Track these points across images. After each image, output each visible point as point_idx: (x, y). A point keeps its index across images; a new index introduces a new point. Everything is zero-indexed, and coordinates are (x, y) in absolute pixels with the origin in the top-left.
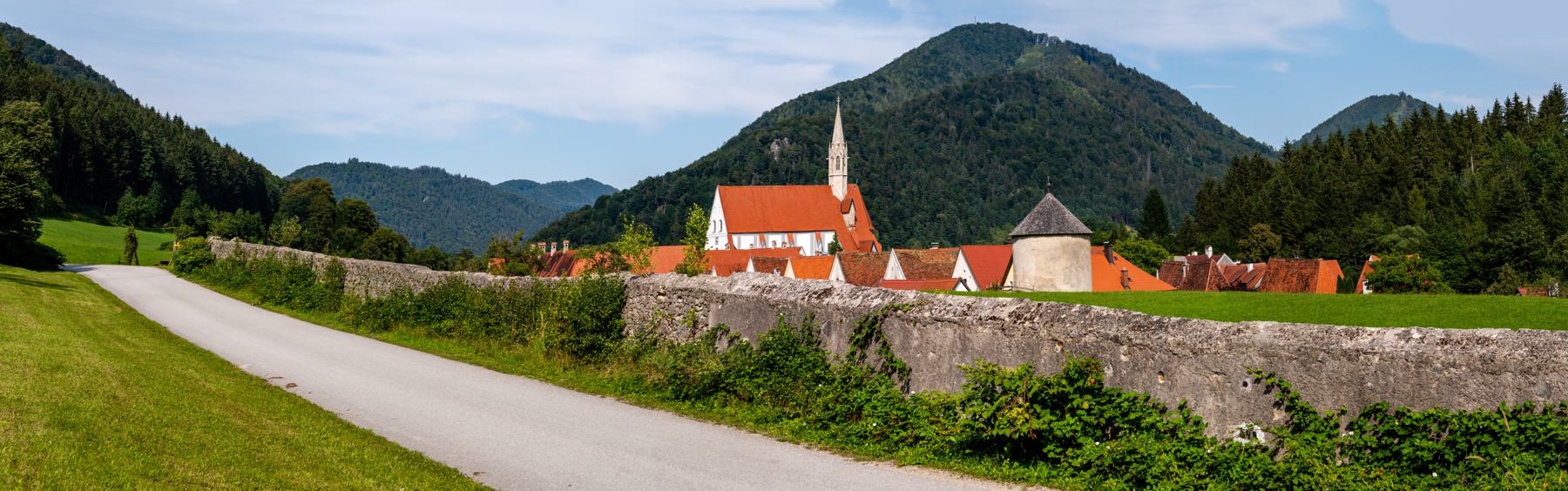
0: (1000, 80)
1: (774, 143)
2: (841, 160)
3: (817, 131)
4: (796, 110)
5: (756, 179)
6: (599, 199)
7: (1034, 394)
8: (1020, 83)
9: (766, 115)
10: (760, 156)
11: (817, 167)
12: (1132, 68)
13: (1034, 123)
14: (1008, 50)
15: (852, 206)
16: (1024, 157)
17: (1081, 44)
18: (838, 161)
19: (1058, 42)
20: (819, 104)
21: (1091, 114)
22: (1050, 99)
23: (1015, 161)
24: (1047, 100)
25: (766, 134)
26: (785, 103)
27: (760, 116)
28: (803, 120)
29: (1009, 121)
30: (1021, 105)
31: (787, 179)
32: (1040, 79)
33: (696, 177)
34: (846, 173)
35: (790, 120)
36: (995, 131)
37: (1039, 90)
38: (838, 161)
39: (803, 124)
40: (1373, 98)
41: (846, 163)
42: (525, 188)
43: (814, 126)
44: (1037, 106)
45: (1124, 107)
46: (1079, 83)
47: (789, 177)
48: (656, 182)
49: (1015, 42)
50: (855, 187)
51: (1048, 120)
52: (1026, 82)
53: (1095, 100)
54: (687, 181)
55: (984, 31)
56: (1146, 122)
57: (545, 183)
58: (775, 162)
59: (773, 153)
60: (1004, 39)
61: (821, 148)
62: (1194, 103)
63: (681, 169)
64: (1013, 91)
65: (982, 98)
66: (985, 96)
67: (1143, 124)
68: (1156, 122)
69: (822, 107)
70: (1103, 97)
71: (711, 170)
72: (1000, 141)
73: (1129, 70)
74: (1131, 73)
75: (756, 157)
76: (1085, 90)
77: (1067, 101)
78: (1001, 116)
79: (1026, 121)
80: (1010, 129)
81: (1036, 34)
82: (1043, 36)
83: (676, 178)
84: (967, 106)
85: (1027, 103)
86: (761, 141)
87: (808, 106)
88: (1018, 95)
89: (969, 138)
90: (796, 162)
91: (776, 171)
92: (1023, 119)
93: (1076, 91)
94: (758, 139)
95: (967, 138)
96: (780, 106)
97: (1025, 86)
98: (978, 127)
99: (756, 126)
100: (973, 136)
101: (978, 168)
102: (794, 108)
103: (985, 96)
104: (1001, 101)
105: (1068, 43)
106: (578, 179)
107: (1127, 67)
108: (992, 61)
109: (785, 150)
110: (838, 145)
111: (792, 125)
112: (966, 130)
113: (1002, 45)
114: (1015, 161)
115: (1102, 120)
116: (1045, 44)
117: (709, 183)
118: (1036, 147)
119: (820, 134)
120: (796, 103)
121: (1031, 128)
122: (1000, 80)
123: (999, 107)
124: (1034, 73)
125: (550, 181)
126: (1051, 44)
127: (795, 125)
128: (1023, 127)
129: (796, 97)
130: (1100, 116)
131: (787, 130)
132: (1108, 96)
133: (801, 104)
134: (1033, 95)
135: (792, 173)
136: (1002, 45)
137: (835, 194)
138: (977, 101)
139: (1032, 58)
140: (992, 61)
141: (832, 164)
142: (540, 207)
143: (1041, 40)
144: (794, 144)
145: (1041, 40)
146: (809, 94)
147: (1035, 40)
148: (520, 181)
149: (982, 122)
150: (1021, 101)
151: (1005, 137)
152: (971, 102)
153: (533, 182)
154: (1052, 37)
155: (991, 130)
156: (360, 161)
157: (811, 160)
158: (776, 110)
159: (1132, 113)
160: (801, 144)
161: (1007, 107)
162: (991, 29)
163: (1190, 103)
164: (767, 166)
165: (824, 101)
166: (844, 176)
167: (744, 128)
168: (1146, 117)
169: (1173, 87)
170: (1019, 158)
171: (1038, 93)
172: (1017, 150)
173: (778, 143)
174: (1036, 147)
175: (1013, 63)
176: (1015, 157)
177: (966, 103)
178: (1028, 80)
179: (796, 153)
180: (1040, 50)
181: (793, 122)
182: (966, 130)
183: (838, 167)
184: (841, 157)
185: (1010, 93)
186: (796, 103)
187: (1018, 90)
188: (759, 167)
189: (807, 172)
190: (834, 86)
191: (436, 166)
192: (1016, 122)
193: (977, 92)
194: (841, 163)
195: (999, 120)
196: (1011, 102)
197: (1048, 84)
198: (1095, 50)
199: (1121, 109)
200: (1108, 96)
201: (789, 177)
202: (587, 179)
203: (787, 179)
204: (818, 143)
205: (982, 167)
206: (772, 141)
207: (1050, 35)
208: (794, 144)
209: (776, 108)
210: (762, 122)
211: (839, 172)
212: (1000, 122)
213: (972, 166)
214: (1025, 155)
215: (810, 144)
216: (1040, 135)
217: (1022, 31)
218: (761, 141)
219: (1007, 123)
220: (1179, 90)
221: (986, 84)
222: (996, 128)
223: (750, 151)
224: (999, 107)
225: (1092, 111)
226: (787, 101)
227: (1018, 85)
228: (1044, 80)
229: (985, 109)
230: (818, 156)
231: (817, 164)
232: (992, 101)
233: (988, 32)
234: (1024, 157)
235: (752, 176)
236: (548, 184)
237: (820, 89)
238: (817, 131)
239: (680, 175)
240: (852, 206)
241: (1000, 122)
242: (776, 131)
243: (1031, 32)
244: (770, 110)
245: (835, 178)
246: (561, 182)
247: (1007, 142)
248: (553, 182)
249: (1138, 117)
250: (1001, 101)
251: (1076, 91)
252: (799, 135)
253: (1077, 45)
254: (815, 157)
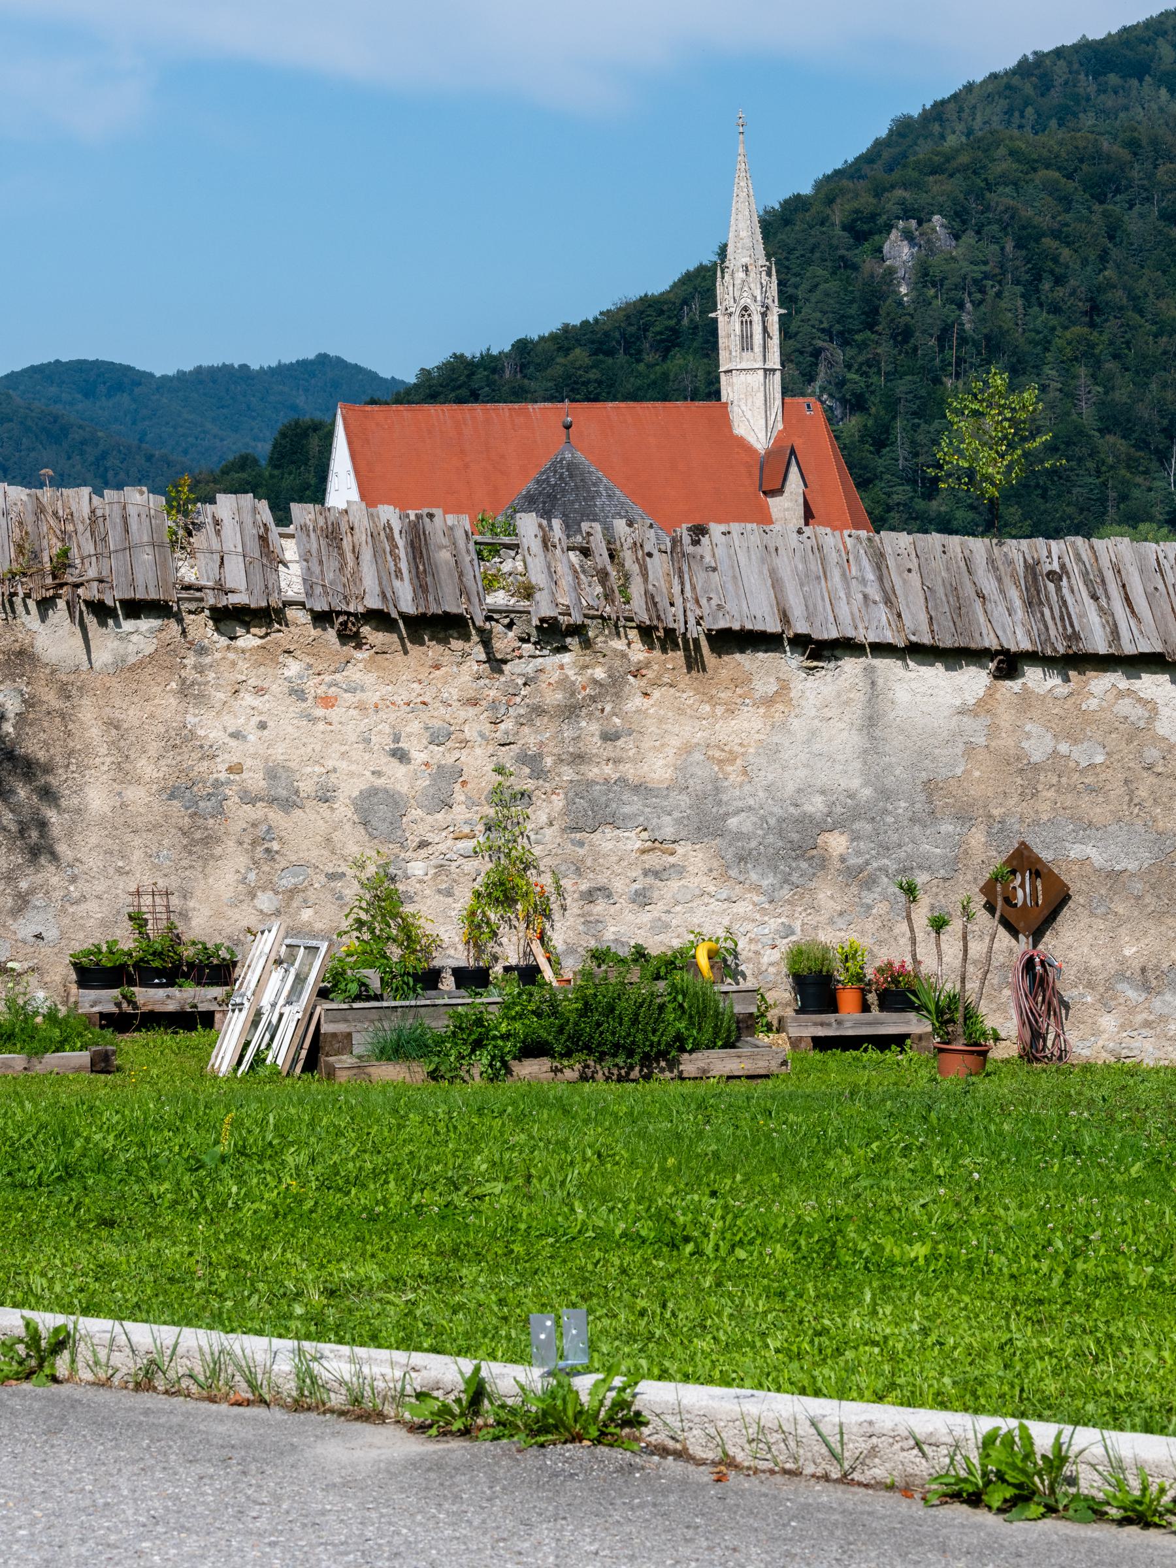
1: (894, 234)
2: (756, 318)
3: (1051, 189)
4: (1009, 112)
5: (830, 365)
6: (283, 435)
9: (904, 129)
10: (848, 281)
11: (1054, 320)
15: (794, 469)
18: (747, 324)
20: (1092, 89)
25: (866, 201)
26: (969, 87)
27: (883, 133)
28: (1002, 151)
31: (945, 364)
33: (621, 358)
34: (775, 361)
35: (957, 151)
38: (747, 324)
39: (1003, 165)
41: (774, 329)
42: (102, 389)
43: (1043, 174)
47: (952, 355)
48: (482, 373)
50: (812, 409)
54: (587, 369)
57: (171, 372)
58: (900, 303)
59: (891, 271)
61: (1066, 253)
63: (566, 329)
69: (1109, 101)
71: (674, 331)
75: (833, 286)
83: (550, 361)
86: (848, 227)
87: (1055, 97)
90: (977, 304)
91: (903, 336)
94: (837, 219)
96: (955, 97)
99: (866, 169)
102: (1003, 104)
106: (289, 358)
109: (933, 260)
110: (746, 269)
111: (965, 168)
117: (665, 376)
119: (1066, 202)
120: (1009, 87)
125: (188, 367)
127: (974, 169)
129: (1011, 63)
131: (941, 188)
133: (1028, 89)
135: (963, 340)
137: (740, 430)
141: (729, 330)
142: (149, 458)
144: (969, 238)
146: (1059, 53)
148: (80, 366)
153: (129, 368)
157: (1031, 293)
158: (938, 113)
160: (995, 240)
164: (870, 319)
165: (1113, 79)
166: (768, 372)
167: (828, 178)
173: (908, 236)
179: (976, 271)
181: (964, 159)
183: (746, 343)
184: (756, 310)
186: (1009, 87)
188: (842, 319)
189: (1018, 337)
190: (1149, 24)
194: (757, 329)
201: (952, 355)
202: (323, 359)
203: (945, 364)
204: (1056, 235)
206: (889, 227)
208: (969, 238)
209: (940, 105)
210: (886, 154)
211: (752, 360)
215: (1027, 238)
218: (848, 227)
223: (809, 262)
226: (979, 79)
230: (1059, 281)
231: (1055, 310)
235: (817, 353)
236: (181, 375)
237: (1096, 34)
238: (1051, 189)
239: (567, 351)
240: (794, 469)
242: (899, 193)
244: (915, 112)
245: (739, 380)
246: (226, 369)
248: (199, 370)
252: (988, 208)
254: (1046, 286)
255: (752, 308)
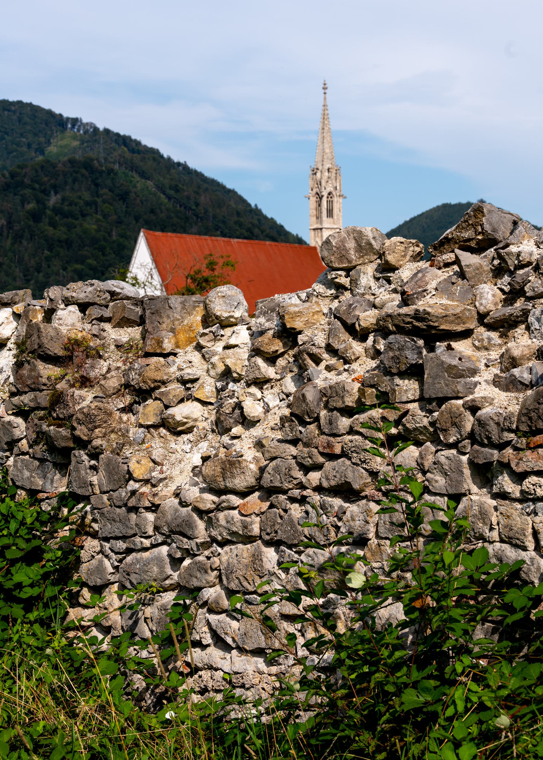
0: (54, 168)
7: (402, 634)
8: (77, 172)
12: (182, 161)
13: (98, 220)
14: (36, 135)
16: (90, 261)
17: (122, 133)
19: (96, 129)
21: (162, 212)
22: (113, 192)
23: (79, 266)
24: (110, 193)
29: (68, 218)
30: (80, 198)
32: (100, 168)
36: (51, 228)
37: (99, 181)
40: (446, 206)
44: (99, 200)
45: (197, 205)
46: (143, 175)
49: (44, 126)
51: (114, 217)
52: (84, 171)
53: (163, 196)
55: (4, 109)
56: (224, 222)
60: (28, 120)
62: (253, 205)
64: (70, 180)
65: (34, 189)
66: (37, 186)
67: (221, 225)
68: (236, 223)
70: (172, 193)
72: (60, 241)
73: (179, 164)
74: (181, 168)
76: (150, 183)
77: (132, 195)
78: (57, 211)
79: (88, 218)
80: (70, 227)
81: (68, 119)
82: (75, 121)
84: (17, 197)
85: (87, 196)
88: (77, 186)
89: (22, 237)
92: (84, 215)
93: (140, 183)
95: (18, 238)
97: (83, 175)
98: (31, 223)
100: (27, 234)
101: (36, 274)
103: (37, 186)
104: (56, 193)
105: (107, 131)
107: (176, 161)
108: (19, 149)
112: (17, 227)
113: (29, 127)
114: (79, 266)
115: (175, 220)
116: (79, 130)
118: (102, 249)
121: (95, 227)
122: (54, 168)
123: (53, 200)
124: (92, 160)
126: (86, 132)
128: (86, 225)
130: (173, 215)
132: (177, 191)
134: (93, 187)
136: (29, 127)
138: (28, 191)
139: (66, 146)
140: (19, 149)
143: (73, 126)
145: (73, 126)
147: (67, 125)
149: (36, 217)
150: (79, 194)
151: (65, 236)
152: (21, 192)
154: (87, 124)
155: (47, 227)
156: (273, 549)
159: (206, 211)
161: (64, 199)
162: (13, 108)
163: (249, 205)
168: (224, 217)
169: (229, 186)
170: (82, 263)
171: (97, 185)
172: (80, 252)
174: (102, 249)
175: (42, 152)
176: (77, 262)
177: (15, 194)
178: (86, 169)
180: (74, 138)
182: (17, 227)
185: (66, 183)
187: (75, 180)
191: (138, 139)
192: (77, 219)
193: (27, 181)
195: (56, 215)
196: (68, 193)
197: (109, 174)
198: (138, 143)
199: (194, 207)
200: (177, 191)
205: (39, 272)
207: (85, 121)
212: (57, 218)
213: (28, 270)
214: (89, 258)
216: (106, 235)
217: (50, 113)
219: (65, 220)
220: (236, 190)
221: (36, 171)
222: (53, 224)
224: (53, 200)
225: (163, 208)
227: (74, 175)
228: (104, 168)
229: (38, 202)
232: (45, 192)
233: (9, 111)
234: (90, 261)
241: (57, 218)
243: (61, 115)
247: (68, 244)
249: (214, 217)
250: (56, 193)
251: (140, 183)
253: (118, 135)
255: (334, 193)
